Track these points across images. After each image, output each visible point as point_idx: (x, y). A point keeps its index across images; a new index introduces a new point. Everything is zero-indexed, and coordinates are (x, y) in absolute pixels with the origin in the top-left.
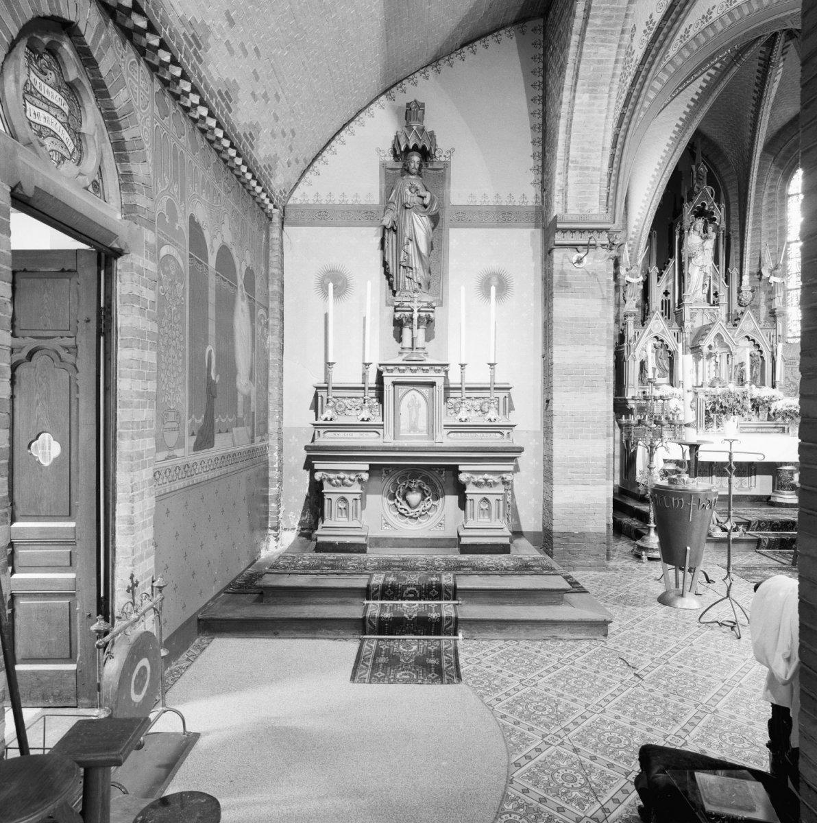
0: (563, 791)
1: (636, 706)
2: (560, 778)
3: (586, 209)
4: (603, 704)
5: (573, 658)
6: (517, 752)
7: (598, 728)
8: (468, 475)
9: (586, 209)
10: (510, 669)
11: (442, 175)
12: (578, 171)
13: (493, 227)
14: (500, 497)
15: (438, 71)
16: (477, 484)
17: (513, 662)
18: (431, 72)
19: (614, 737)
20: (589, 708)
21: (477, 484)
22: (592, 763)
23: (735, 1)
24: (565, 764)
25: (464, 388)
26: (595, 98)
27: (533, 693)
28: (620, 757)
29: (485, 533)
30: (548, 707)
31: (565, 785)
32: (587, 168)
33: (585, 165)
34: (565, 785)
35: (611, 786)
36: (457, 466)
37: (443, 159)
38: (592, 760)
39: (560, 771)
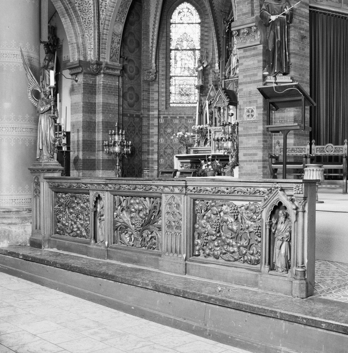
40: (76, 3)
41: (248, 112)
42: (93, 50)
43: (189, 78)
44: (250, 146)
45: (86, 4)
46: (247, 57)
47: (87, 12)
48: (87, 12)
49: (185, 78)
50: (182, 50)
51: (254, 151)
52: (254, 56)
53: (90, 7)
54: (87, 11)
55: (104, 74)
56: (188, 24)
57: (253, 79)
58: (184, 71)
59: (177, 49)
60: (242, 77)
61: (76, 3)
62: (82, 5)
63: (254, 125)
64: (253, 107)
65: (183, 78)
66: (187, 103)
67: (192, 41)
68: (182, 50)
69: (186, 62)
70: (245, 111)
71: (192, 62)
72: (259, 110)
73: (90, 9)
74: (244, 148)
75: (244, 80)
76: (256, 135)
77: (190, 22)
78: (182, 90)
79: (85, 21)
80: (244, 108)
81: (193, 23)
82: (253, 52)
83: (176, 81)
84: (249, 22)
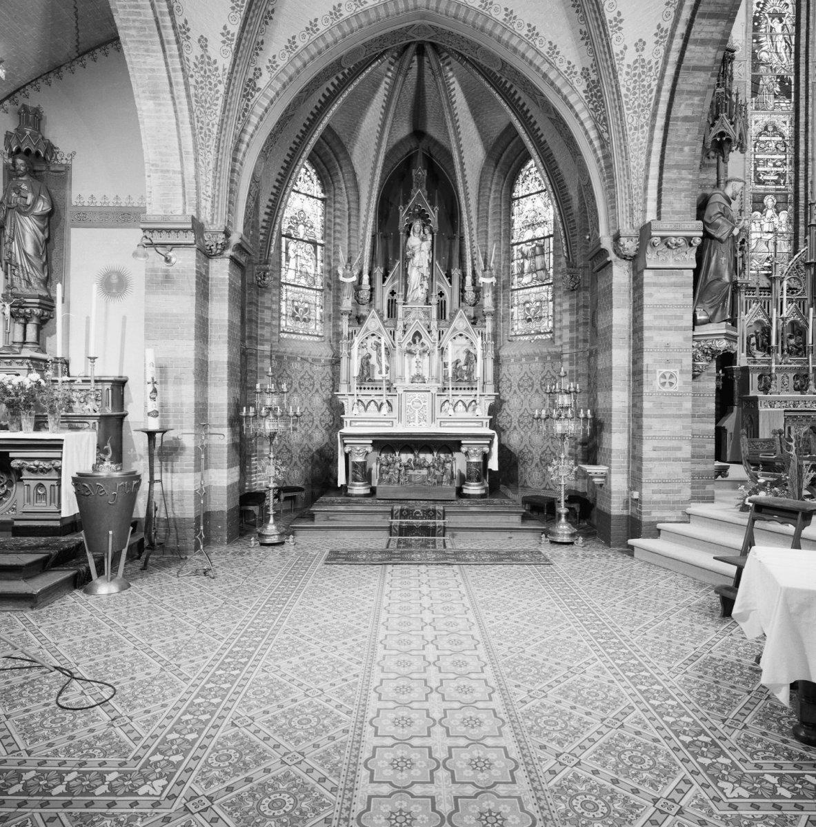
0: (584, 822)
1: (619, 757)
2: (579, 806)
3: (170, 209)
4: (621, 717)
5: (584, 666)
6: (580, 734)
7: (658, 775)
8: (19, 461)
9: (170, 209)
10: (516, 679)
11: (63, 175)
12: (160, 174)
13: (112, 227)
14: (55, 483)
15: (60, 78)
16: (30, 470)
17: (519, 671)
18: (52, 78)
19: (636, 756)
20: (605, 722)
21: (30, 470)
22: (614, 787)
23: (365, 2)
24: (584, 788)
25: (93, 382)
26: (160, 104)
27: (543, 706)
28: (644, 781)
29: (36, 517)
30: (560, 721)
31: (585, 814)
32: (168, 171)
33: (165, 168)
34: (585, 814)
35: (638, 816)
36: (8, 453)
37: (64, 162)
38: (613, 784)
39: (578, 797)
40: (192, 76)
41: (671, 376)
42: (210, 199)
43: (307, 291)
44: (667, 434)
45: (210, 89)
46: (661, 285)
47: (209, 108)
48: (209, 108)
49: (301, 289)
50: (298, 240)
51: (674, 443)
52: (675, 285)
53: (217, 99)
54: (208, 105)
55: (232, 258)
56: (308, 195)
57: (675, 323)
58: (299, 277)
59: (288, 236)
60: (652, 318)
61: (192, 76)
62: (202, 88)
63: (675, 400)
64: (675, 370)
65: (299, 289)
66: (304, 334)
67: (312, 227)
68: (298, 240)
69: (303, 262)
70: (658, 376)
71: (312, 263)
72: (684, 376)
73: (216, 105)
74: (653, 438)
75: (656, 323)
76: (679, 416)
77: (309, 193)
78: (297, 310)
79: (201, 128)
80: (655, 372)
81: (313, 197)
82: (673, 279)
83: (289, 293)
84: (690, 227)
